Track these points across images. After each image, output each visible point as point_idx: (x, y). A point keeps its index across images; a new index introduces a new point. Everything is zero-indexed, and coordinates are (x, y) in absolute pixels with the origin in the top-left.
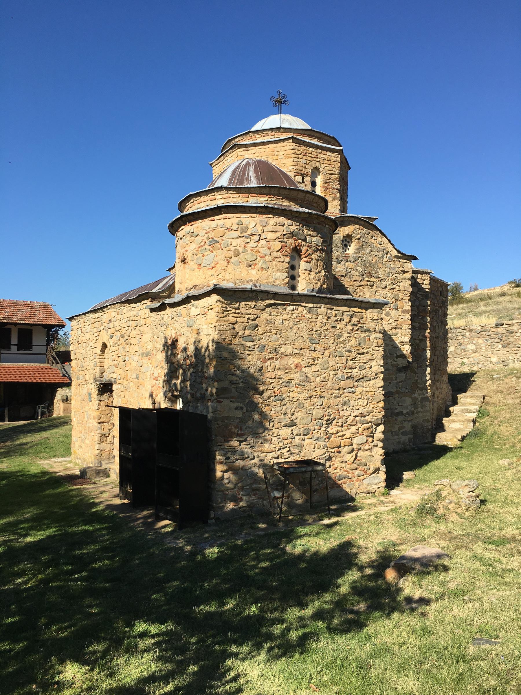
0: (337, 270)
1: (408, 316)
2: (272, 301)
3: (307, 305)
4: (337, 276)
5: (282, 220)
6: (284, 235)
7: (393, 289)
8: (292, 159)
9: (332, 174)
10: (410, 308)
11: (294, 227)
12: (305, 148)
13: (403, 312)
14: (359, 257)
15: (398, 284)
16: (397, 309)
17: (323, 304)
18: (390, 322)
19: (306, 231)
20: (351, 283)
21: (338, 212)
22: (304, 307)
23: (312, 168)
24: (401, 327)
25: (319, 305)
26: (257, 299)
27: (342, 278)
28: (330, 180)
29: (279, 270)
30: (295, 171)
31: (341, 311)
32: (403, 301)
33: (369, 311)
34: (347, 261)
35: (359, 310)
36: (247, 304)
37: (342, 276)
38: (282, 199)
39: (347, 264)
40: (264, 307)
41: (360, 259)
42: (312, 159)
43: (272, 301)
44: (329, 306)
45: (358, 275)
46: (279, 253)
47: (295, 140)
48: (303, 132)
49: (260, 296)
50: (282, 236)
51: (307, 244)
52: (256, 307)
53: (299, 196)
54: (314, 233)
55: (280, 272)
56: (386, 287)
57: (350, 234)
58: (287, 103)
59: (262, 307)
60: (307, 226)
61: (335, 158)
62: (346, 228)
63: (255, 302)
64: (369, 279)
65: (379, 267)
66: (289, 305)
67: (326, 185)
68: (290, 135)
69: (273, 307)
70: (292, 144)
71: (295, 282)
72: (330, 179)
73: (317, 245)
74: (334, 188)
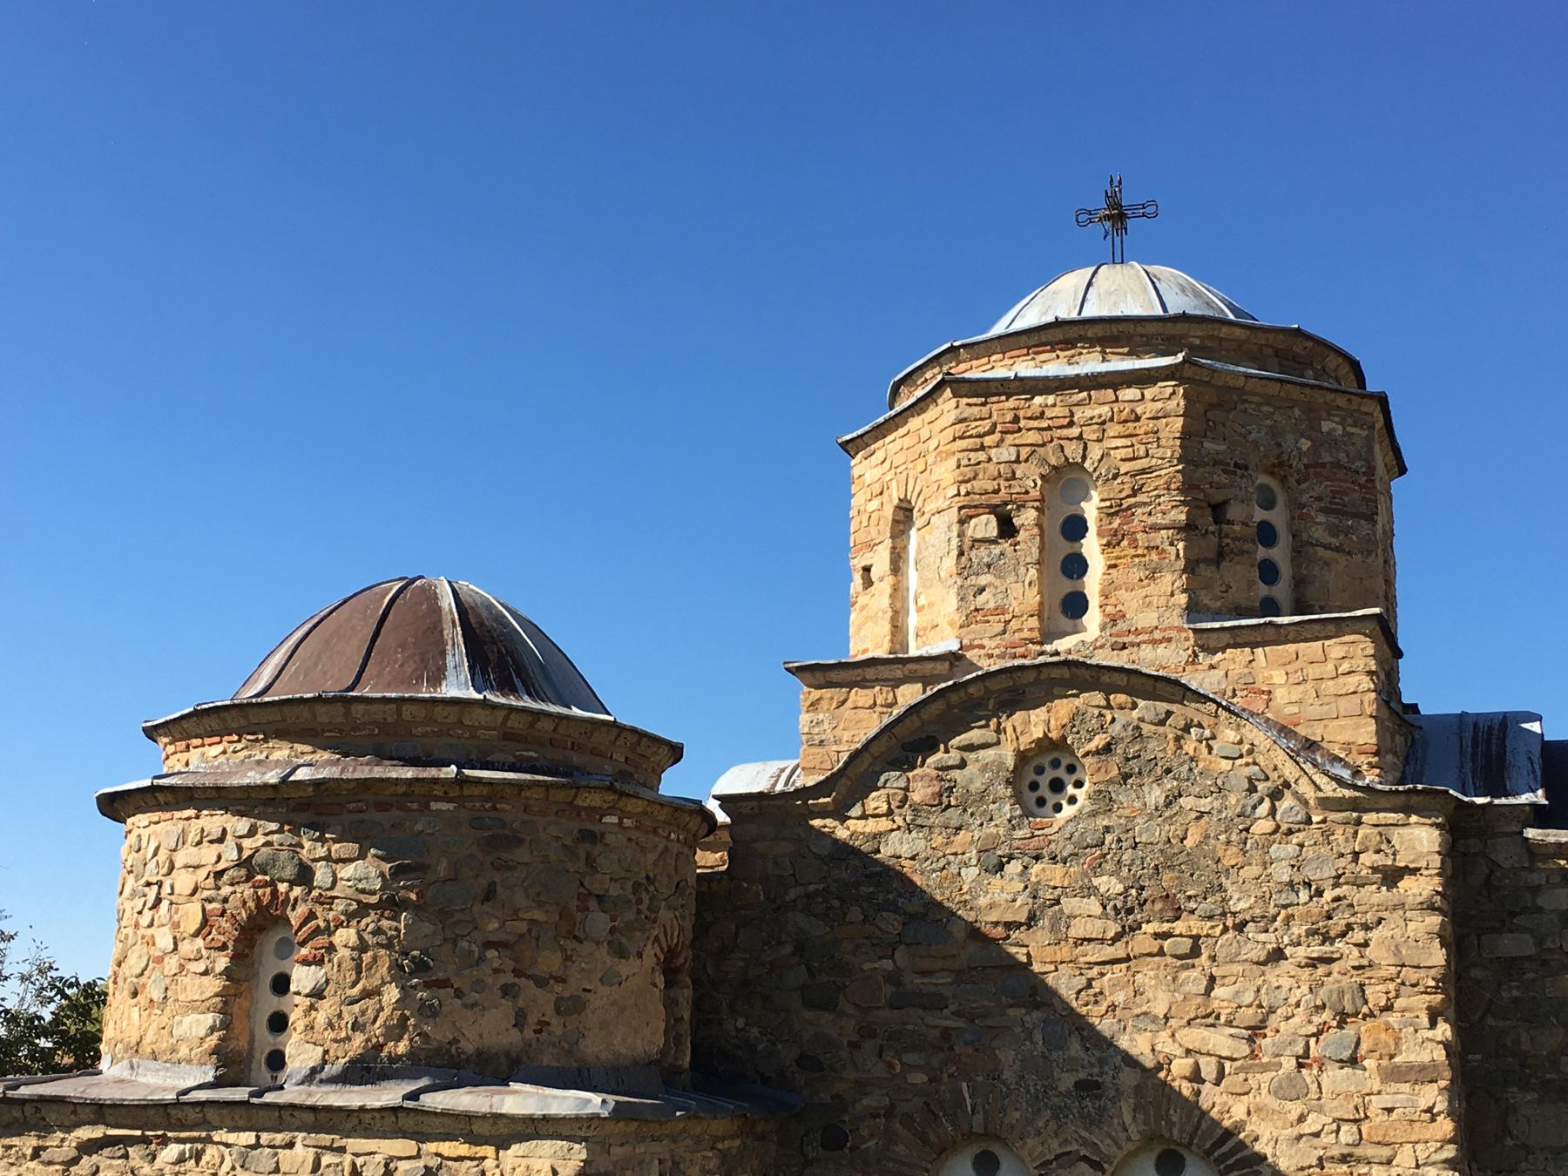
0: (983, 901)
1: (1432, 1095)
2: (97, 1132)
3: (231, 1138)
4: (986, 929)
5: (214, 821)
6: (219, 875)
7: (1329, 961)
8: (953, 462)
9: (1143, 471)
10: (1440, 1055)
11: (265, 837)
12: (1012, 403)
13: (1395, 1074)
14: (1107, 829)
15: (1358, 936)
16: (1353, 1061)
17: (299, 1129)
18: (1311, 1125)
19: (307, 844)
20: (1065, 952)
21: (1178, 622)
22: (227, 1145)
23: (1045, 470)
24: (1385, 1152)
25: (279, 1138)
26: (45, 1129)
27: (1015, 935)
28: (1141, 498)
29: (192, 1006)
30: (962, 501)
31: (378, 1158)
32: (1393, 1019)
33: (516, 1149)
34: (1037, 858)
35: (463, 1149)
36: (11, 1147)
37: (1009, 926)
38: (265, 740)
39: (1036, 868)
40: (74, 1153)
41: (1109, 838)
42: (1047, 435)
43: (97, 1132)
44: (325, 1139)
45: (1098, 910)
46: (199, 942)
47: (963, 388)
48: (1035, 339)
49: (52, 1116)
50: (211, 880)
51: (315, 893)
52: (44, 1155)
53: (324, 719)
54: (349, 848)
55: (195, 1010)
56: (1277, 955)
57: (1054, 735)
58: (1148, 210)
59: (68, 1151)
60: (312, 826)
61: (1159, 405)
62: (1038, 715)
63: (39, 1137)
64: (1166, 927)
65: (1227, 862)
66: (164, 1141)
67: (1117, 522)
68: (934, 376)
69: (106, 1152)
70: (953, 402)
71: (281, 1038)
72: (1134, 493)
73: (363, 891)
74: (1156, 528)
